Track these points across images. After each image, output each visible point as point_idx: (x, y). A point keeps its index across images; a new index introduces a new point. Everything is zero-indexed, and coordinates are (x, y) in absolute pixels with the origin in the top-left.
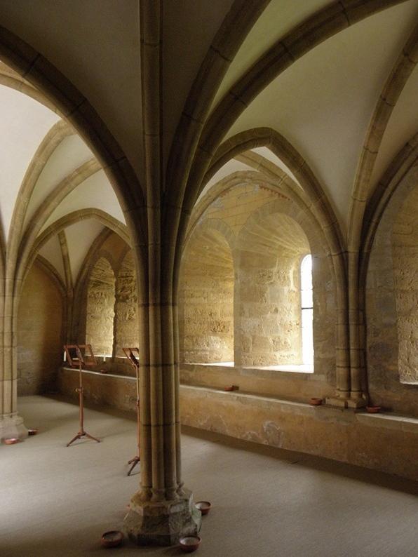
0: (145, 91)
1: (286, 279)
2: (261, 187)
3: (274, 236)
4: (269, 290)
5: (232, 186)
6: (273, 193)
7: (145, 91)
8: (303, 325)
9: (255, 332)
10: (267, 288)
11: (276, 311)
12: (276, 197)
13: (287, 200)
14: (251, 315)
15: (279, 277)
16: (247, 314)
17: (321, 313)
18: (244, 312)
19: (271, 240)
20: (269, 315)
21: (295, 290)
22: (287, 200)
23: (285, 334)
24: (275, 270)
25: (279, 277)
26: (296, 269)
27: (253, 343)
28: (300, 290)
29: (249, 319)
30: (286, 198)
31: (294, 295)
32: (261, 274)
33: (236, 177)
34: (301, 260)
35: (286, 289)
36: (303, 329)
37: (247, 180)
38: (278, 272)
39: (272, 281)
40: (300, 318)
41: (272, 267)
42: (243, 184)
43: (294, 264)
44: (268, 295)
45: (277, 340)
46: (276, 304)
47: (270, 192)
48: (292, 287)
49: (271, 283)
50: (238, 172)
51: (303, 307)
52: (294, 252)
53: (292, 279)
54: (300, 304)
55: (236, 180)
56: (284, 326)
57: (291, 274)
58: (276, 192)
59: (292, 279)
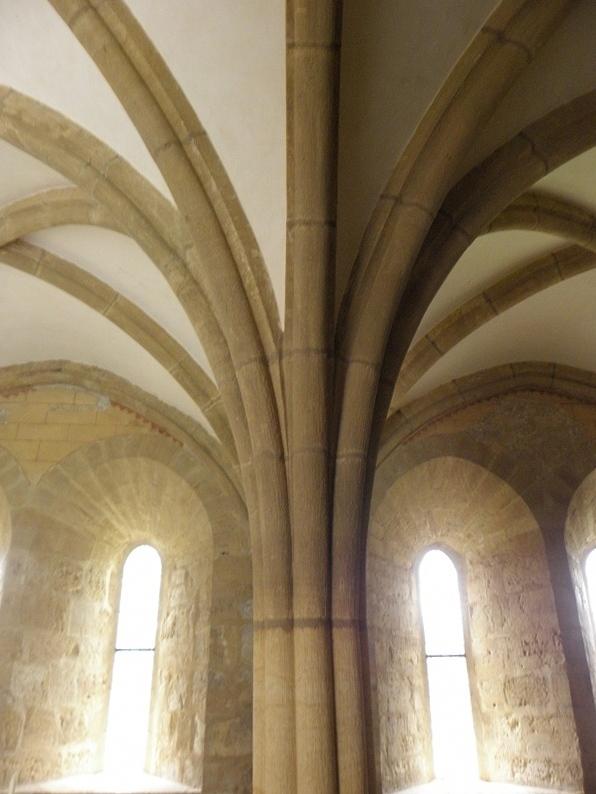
0: (297, 131)
1: (99, 585)
2: (114, 404)
3: (107, 499)
4: (72, 603)
5: (41, 384)
6: (141, 421)
7: (297, 131)
8: (113, 685)
9: (34, 699)
10: (68, 601)
11: (76, 651)
12: (146, 430)
13: (171, 439)
14: (33, 659)
15: (90, 582)
16: (26, 656)
17: (228, 661)
18: (21, 651)
19: (97, 505)
20: (63, 661)
21: (110, 610)
22: (171, 439)
23: (83, 702)
24: (87, 565)
25: (90, 582)
26: (116, 571)
27: (25, 727)
28: (116, 611)
29: (27, 669)
30: (168, 435)
31: (106, 620)
32: (64, 569)
33: (59, 370)
34: (126, 553)
35: (97, 607)
36: (113, 691)
37: (88, 383)
38: (91, 571)
39: (79, 588)
40: (110, 670)
41: (83, 559)
42: (71, 387)
43: (116, 557)
44: (68, 618)
45: (68, 717)
46: (78, 635)
47: (132, 417)
48: (106, 605)
49: (77, 591)
50: (66, 362)
51: (152, 652)
52: (121, 536)
53: (107, 588)
54: (423, 650)
55: (59, 376)
56: (83, 684)
57: (107, 579)
58: (146, 421)
59: (107, 588)
